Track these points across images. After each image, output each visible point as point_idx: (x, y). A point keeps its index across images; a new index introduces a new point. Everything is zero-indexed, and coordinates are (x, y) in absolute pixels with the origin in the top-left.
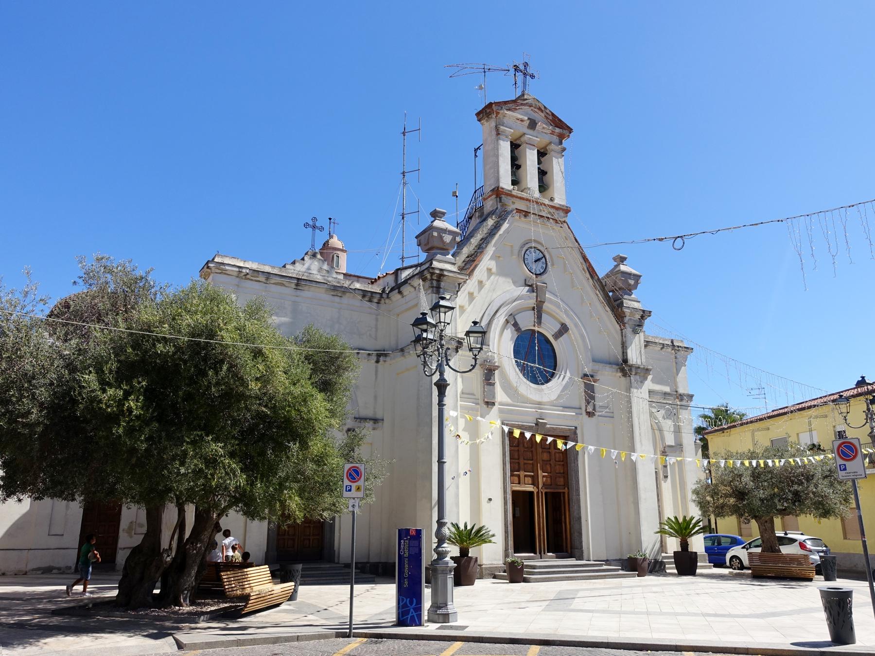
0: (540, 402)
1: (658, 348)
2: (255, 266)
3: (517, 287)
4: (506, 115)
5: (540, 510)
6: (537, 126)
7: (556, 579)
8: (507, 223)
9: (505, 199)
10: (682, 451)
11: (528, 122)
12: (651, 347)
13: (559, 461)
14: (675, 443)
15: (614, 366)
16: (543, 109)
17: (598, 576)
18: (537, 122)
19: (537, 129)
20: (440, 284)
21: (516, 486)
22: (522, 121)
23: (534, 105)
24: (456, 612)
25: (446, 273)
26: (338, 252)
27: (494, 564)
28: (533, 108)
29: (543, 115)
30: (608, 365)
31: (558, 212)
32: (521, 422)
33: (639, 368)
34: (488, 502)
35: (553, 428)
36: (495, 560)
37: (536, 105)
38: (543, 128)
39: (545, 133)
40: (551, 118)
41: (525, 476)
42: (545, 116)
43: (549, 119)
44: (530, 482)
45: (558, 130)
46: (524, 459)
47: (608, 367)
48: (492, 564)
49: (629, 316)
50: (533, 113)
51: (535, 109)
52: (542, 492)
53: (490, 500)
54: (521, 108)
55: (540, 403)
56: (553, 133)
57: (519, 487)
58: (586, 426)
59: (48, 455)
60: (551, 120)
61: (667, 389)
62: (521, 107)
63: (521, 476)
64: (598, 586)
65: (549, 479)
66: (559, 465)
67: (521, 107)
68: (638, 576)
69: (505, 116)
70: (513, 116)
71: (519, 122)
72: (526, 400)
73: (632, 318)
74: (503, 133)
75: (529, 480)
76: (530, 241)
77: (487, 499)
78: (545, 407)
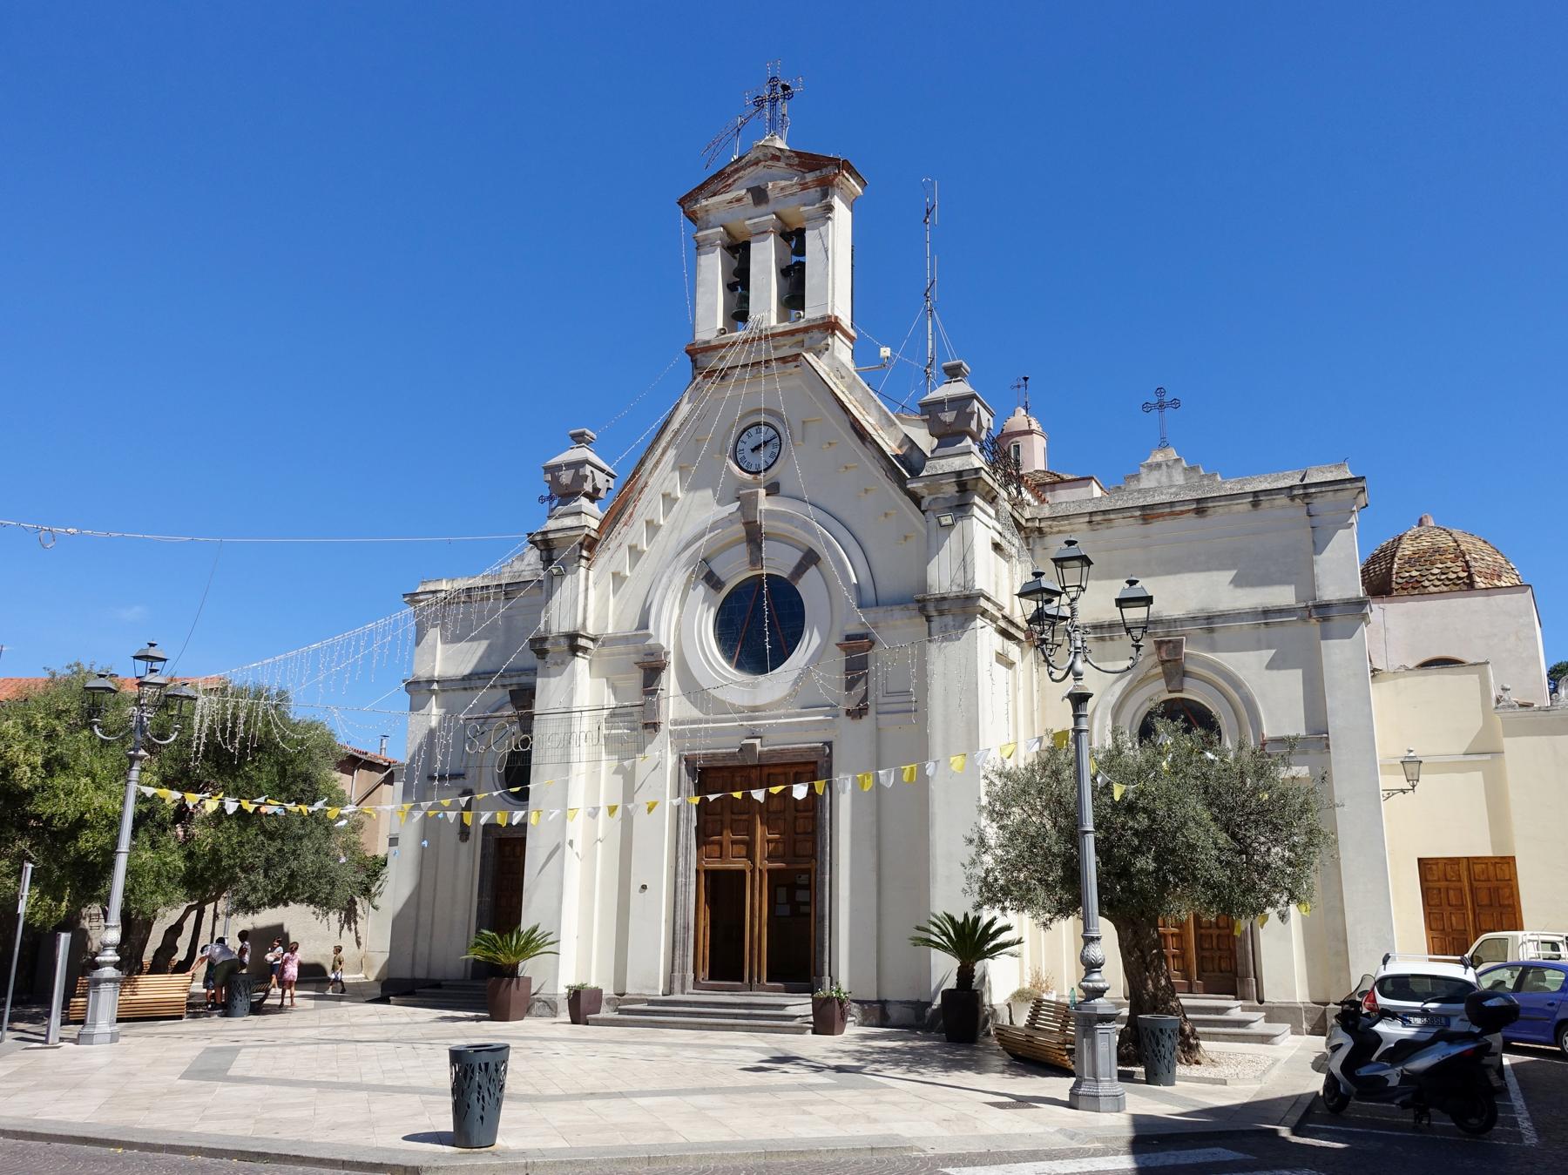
0: (755, 707)
1: (1244, 505)
2: (462, 584)
3: (723, 506)
4: (707, 208)
5: (757, 906)
6: (769, 193)
7: (633, 1024)
8: (688, 403)
9: (703, 359)
10: (1328, 746)
11: (749, 195)
12: (1220, 510)
13: (805, 811)
14: (1307, 729)
15: (911, 606)
16: (778, 153)
17: (718, 1025)
18: (763, 187)
19: (770, 197)
20: (552, 554)
21: (714, 862)
22: (739, 200)
23: (762, 158)
24: (119, 1020)
25: (551, 536)
26: (1018, 439)
27: (645, 995)
28: (763, 163)
29: (782, 164)
30: (898, 607)
31: (811, 334)
32: (726, 748)
33: (944, 599)
34: (640, 892)
35: (774, 750)
36: (647, 987)
37: (765, 155)
38: (782, 189)
39: (792, 194)
40: (796, 161)
41: (733, 842)
42: (787, 164)
43: (794, 166)
44: (744, 853)
45: (810, 177)
46: (733, 813)
47: (897, 612)
48: (641, 994)
49: (929, 494)
50: (768, 170)
51: (767, 163)
52: (760, 871)
53: (644, 887)
54: (740, 178)
55: (755, 709)
56: (804, 187)
57: (721, 863)
58: (850, 740)
59: (1140, 842)
60: (798, 165)
61: (1284, 596)
62: (736, 177)
63: (724, 843)
64: (725, 1037)
65: (781, 846)
66: (806, 818)
67: (736, 177)
68: (814, 1032)
69: (707, 211)
70: (720, 203)
71: (735, 205)
72: (722, 707)
73: (939, 496)
74: (706, 242)
75: (743, 850)
76: (758, 411)
77: (640, 887)
78: (763, 714)
